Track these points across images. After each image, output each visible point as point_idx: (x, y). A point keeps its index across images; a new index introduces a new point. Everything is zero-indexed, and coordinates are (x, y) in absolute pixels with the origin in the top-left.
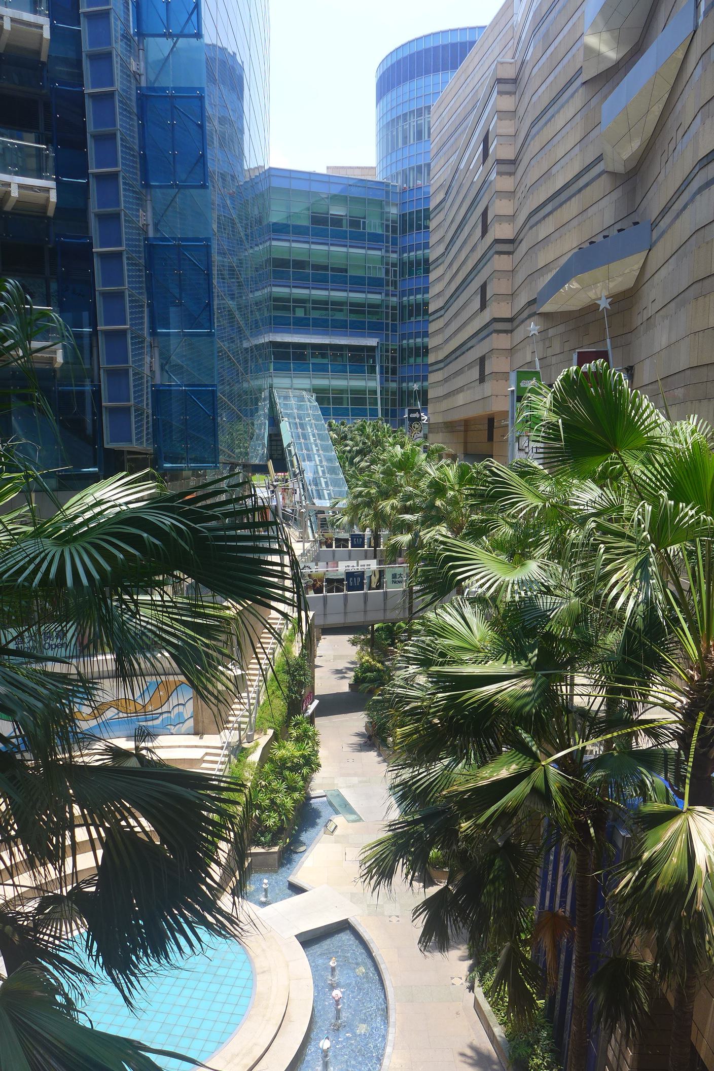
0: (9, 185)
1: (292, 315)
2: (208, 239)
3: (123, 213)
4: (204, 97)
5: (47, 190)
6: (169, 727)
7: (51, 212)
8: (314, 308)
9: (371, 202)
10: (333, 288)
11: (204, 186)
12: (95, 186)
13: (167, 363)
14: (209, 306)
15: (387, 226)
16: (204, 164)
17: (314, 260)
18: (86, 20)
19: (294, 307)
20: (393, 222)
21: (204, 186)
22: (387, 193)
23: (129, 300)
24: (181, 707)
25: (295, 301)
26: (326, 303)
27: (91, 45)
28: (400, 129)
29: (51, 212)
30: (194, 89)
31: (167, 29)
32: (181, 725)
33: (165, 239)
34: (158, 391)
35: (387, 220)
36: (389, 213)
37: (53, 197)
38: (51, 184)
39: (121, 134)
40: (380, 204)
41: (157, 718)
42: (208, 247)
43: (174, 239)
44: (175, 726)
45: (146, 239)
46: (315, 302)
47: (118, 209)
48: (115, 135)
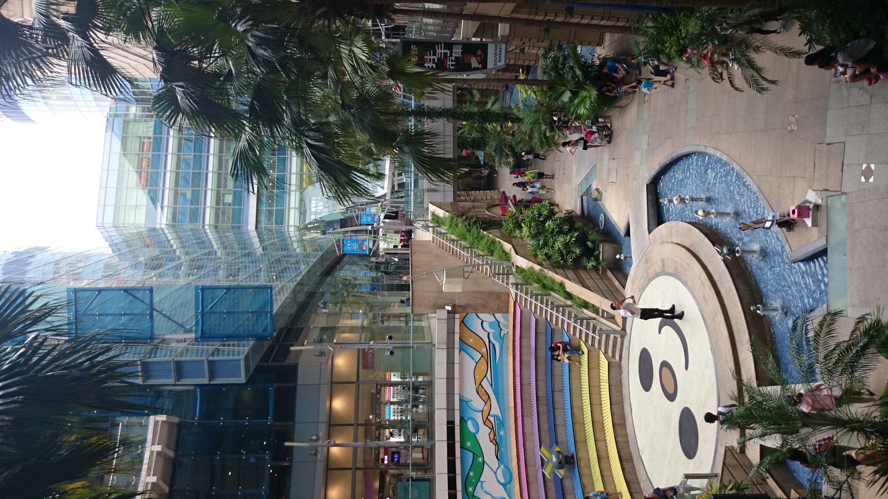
0: (152, 452)
1: (232, 207)
2: (197, 288)
3: (176, 359)
4: (202, 287)
5: (156, 422)
6: (502, 336)
7: (176, 420)
8: (225, 187)
9: (125, 130)
10: (205, 168)
11: (151, 290)
12: (219, 379)
13: (183, 327)
14: (228, 289)
15: (147, 116)
16: (135, 289)
17: (215, 187)
18: (216, 379)
19: (224, 204)
20: (143, 111)
21: (151, 290)
22: (116, 116)
23: (228, 356)
24: (484, 323)
25: (218, 203)
26: (219, 175)
27: (204, 377)
28: (57, 102)
29: (176, 420)
30: (197, 294)
31: (147, 315)
32: (501, 324)
33: (197, 324)
34: (202, 337)
35: (142, 116)
36: (135, 115)
37: (162, 418)
38: (152, 418)
39: (177, 356)
40: (126, 123)
41: (494, 345)
42: (204, 289)
43: (197, 317)
44: (501, 330)
45: (196, 339)
46: (219, 186)
47: (172, 363)
48: (177, 362)
